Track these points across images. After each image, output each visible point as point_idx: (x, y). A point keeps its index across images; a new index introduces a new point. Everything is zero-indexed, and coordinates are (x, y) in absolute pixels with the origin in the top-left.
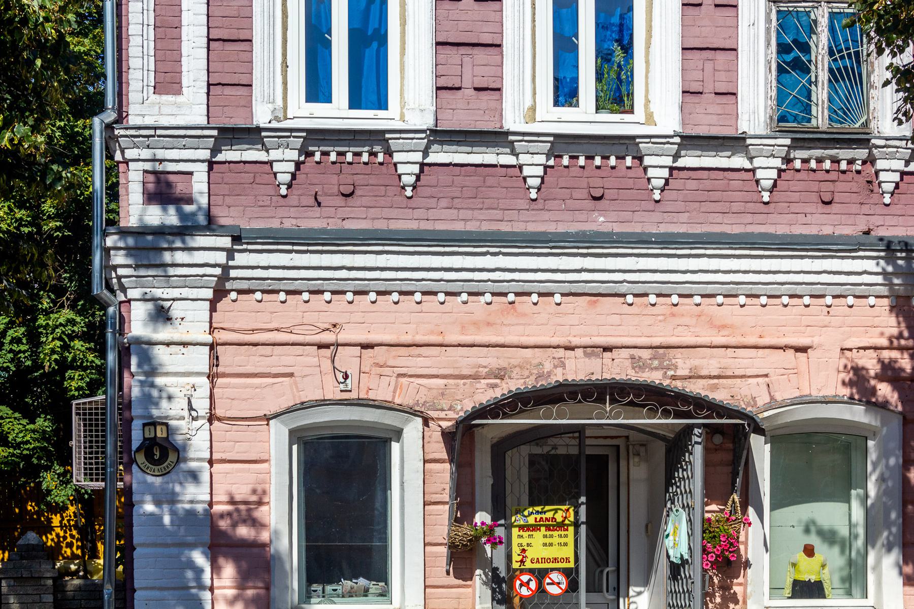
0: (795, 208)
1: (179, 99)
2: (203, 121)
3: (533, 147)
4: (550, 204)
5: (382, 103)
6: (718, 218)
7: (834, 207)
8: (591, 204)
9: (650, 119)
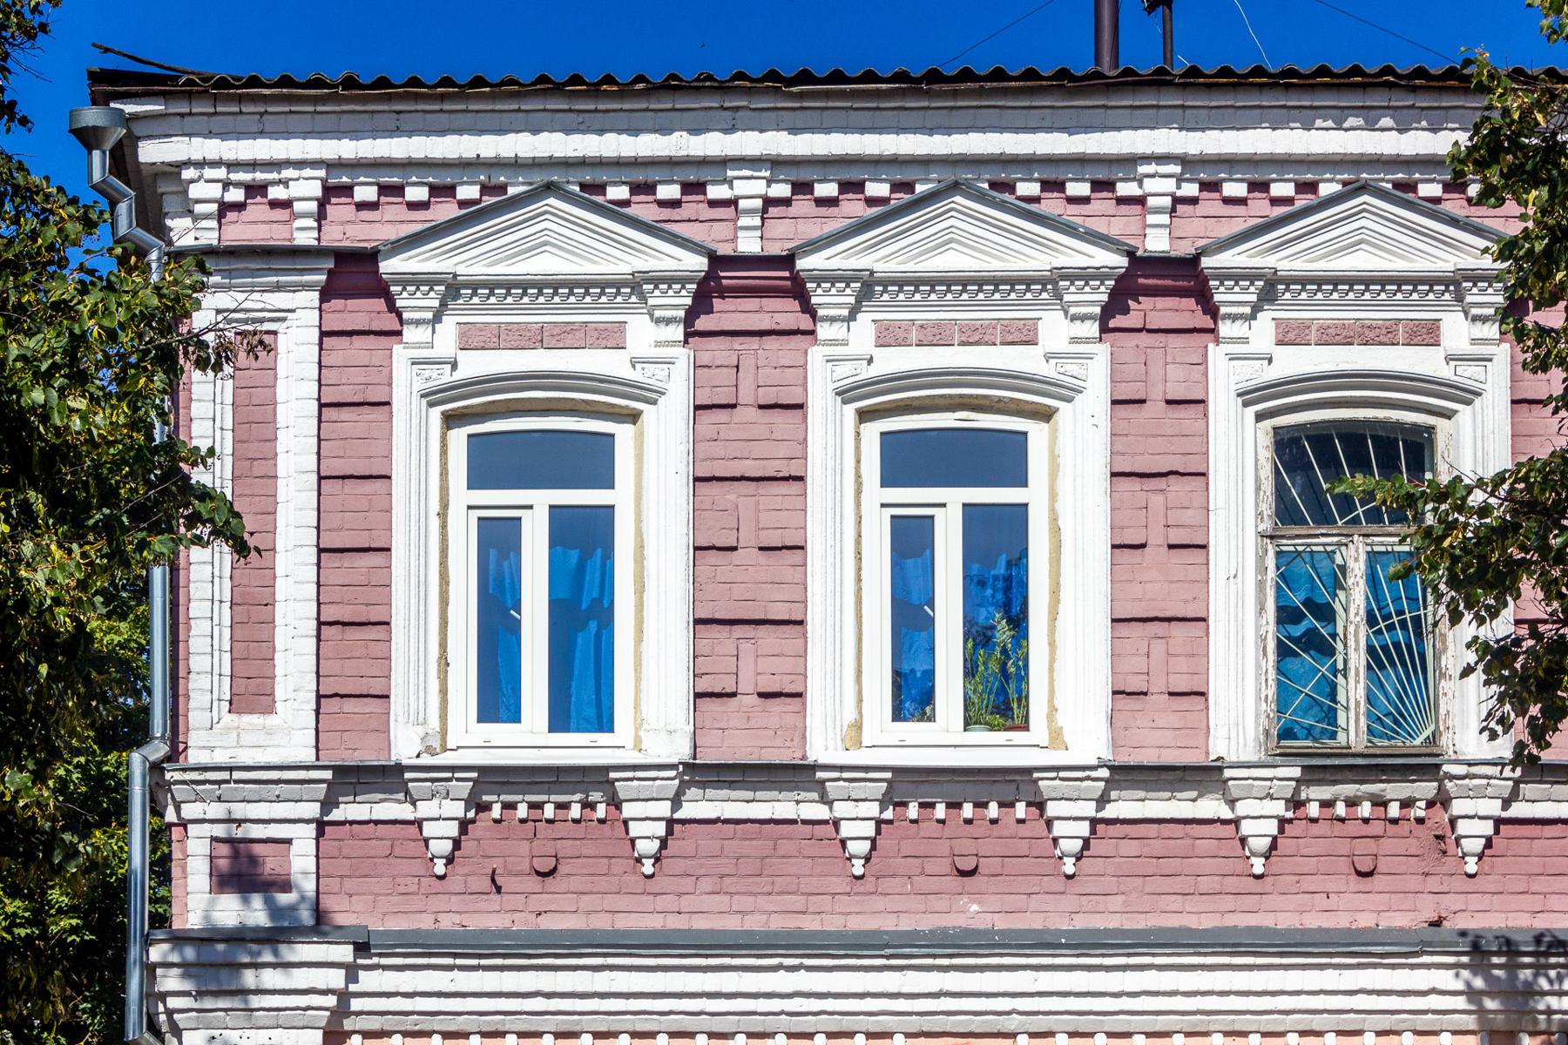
0: (1308, 883)
1: (270, 720)
2: (308, 756)
3: (858, 790)
4: (886, 884)
5: (603, 721)
6: (1175, 902)
7: (1377, 882)
8: (955, 882)
9: (1057, 739)
